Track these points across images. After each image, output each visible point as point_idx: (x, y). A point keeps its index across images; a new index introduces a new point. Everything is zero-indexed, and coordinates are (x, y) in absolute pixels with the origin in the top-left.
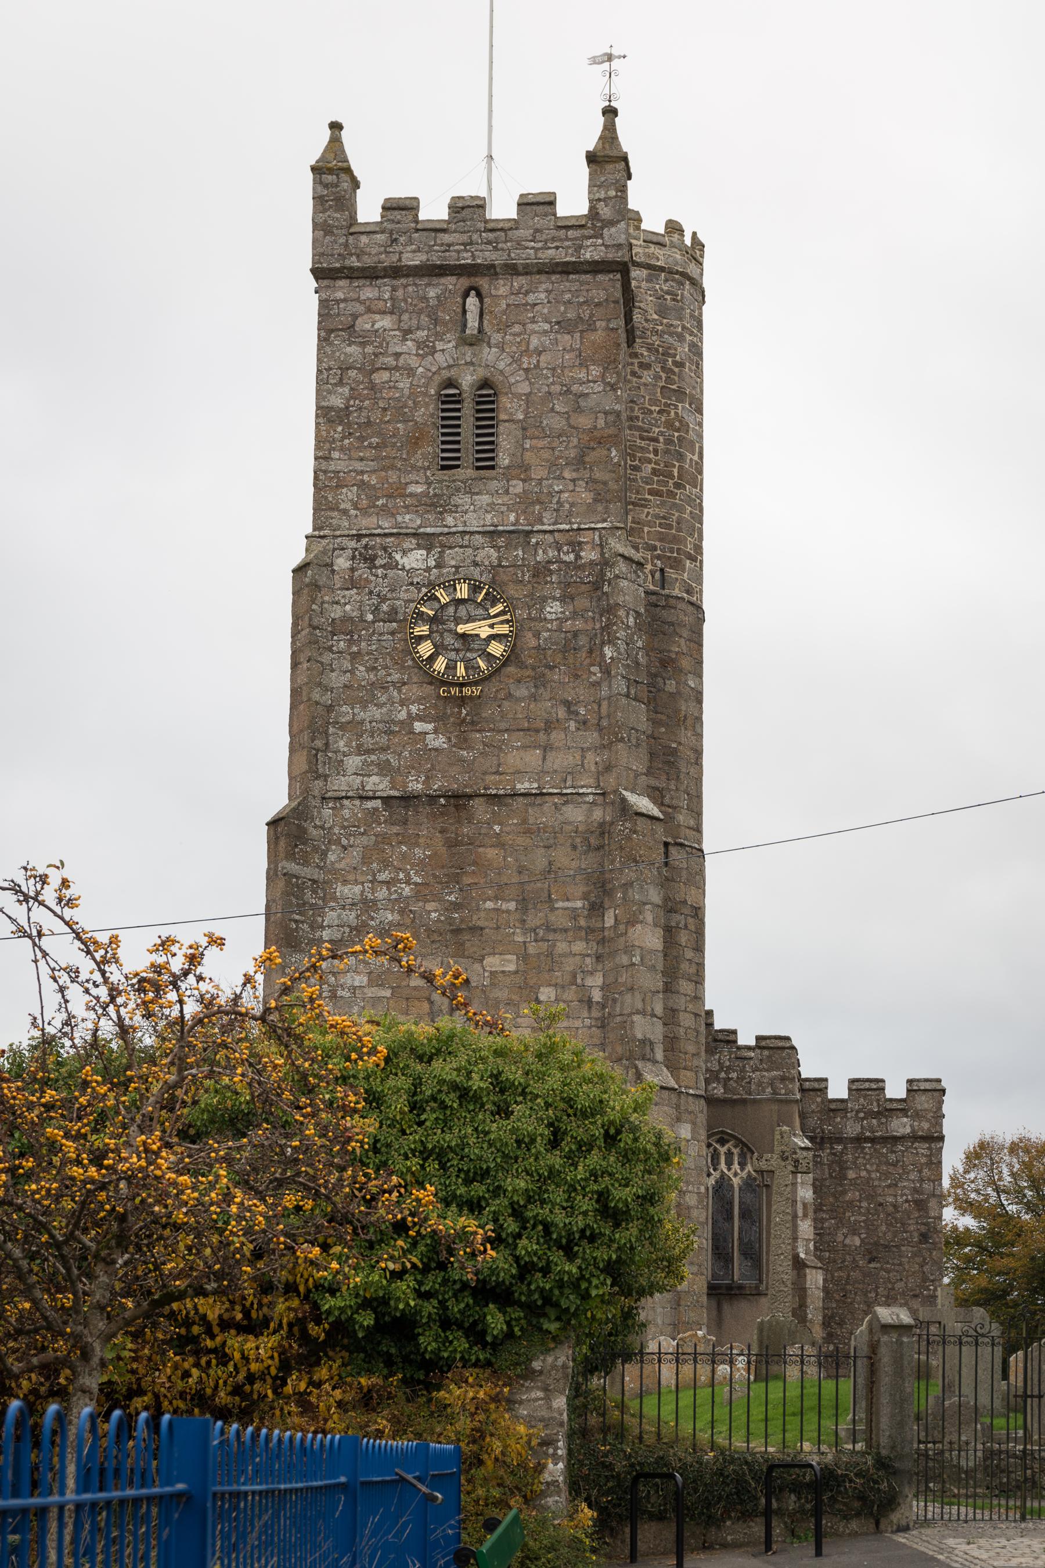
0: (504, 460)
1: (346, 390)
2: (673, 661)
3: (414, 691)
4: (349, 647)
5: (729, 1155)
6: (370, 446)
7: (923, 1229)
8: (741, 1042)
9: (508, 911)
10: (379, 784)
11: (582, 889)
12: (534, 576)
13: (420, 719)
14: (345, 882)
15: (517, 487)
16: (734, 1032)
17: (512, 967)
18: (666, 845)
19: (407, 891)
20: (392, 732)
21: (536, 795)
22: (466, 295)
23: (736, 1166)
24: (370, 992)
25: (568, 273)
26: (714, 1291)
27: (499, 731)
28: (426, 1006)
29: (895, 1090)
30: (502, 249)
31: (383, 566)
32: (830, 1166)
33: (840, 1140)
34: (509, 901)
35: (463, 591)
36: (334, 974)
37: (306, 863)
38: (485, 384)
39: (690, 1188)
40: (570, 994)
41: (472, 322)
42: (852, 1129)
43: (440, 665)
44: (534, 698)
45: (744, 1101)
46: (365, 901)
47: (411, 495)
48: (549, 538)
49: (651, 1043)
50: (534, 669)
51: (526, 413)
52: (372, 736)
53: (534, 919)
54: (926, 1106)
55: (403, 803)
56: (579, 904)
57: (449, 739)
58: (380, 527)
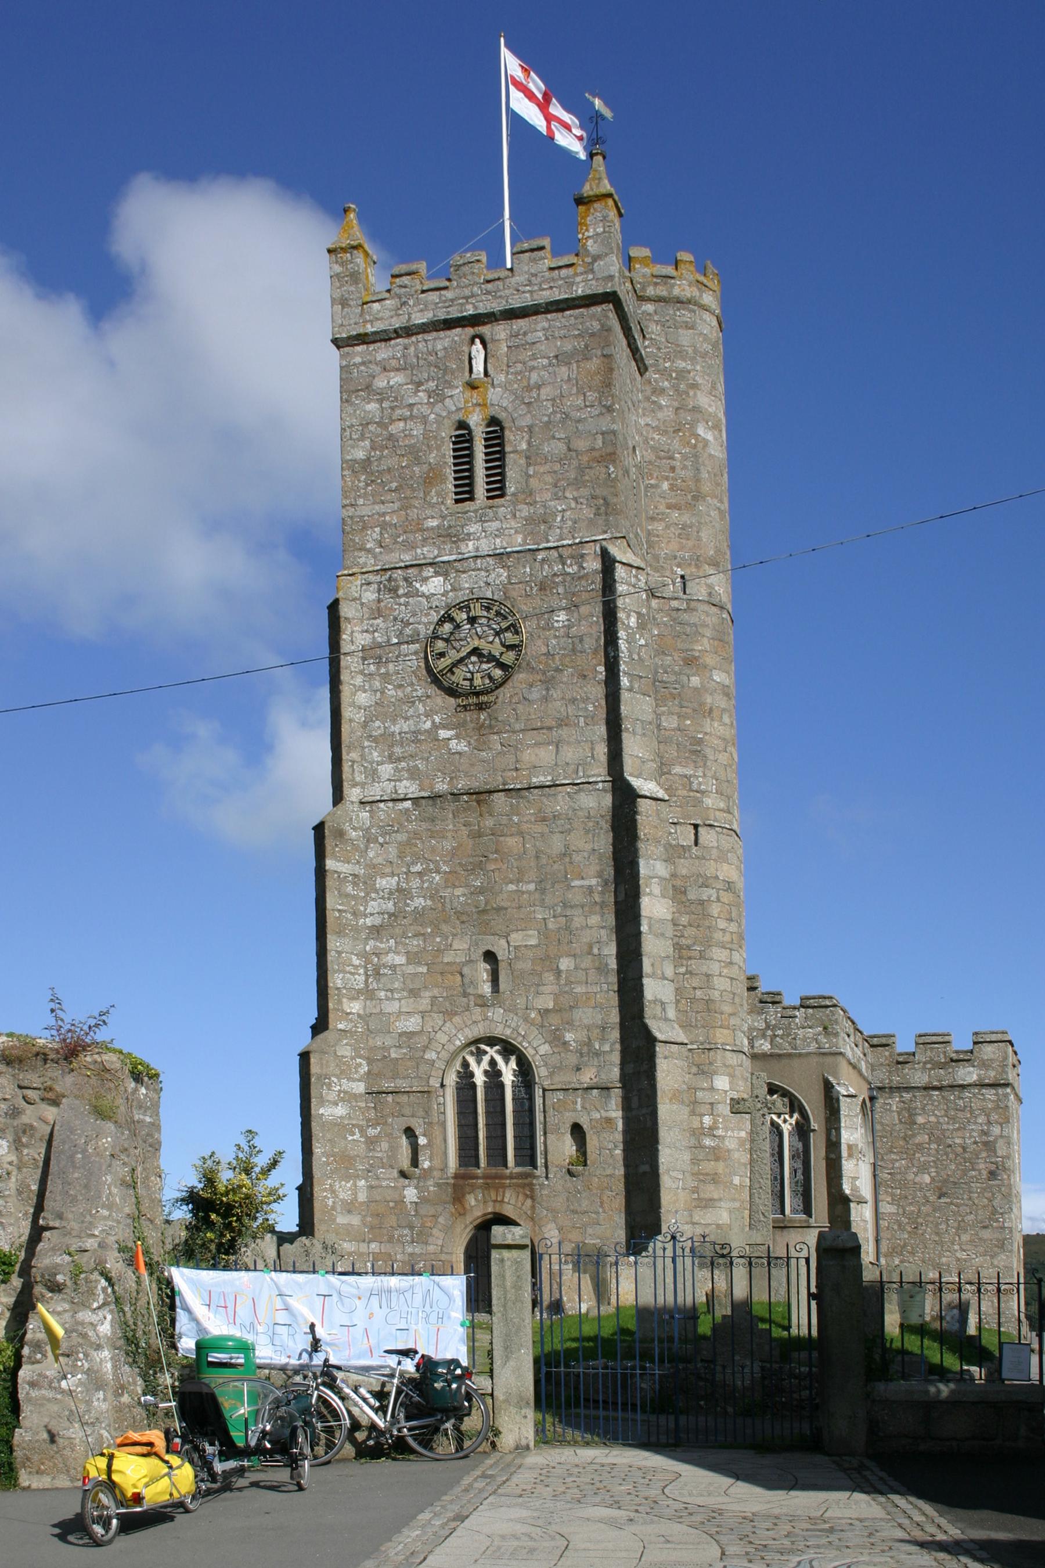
0: (511, 488)
1: (367, 443)
2: (696, 658)
4: (378, 669)
6: (391, 491)
7: (993, 1167)
8: (786, 1002)
9: (529, 892)
10: (409, 787)
12: (541, 590)
13: (445, 727)
14: (384, 875)
15: (524, 511)
18: (696, 826)
20: (419, 741)
21: (549, 787)
22: (472, 342)
24: (410, 969)
25: (563, 310)
27: (514, 732)
28: (459, 978)
30: (500, 297)
31: (406, 595)
32: (899, 1113)
33: (908, 1089)
34: (530, 882)
36: (377, 955)
39: (729, 1133)
40: (587, 962)
41: (479, 366)
44: (546, 699)
45: (790, 1055)
46: (399, 890)
47: (428, 529)
48: (554, 554)
49: (662, 1003)
50: (544, 673)
51: (529, 443)
52: (402, 746)
54: (992, 1056)
55: (430, 802)
56: (594, 882)
57: (469, 743)
58: (402, 561)
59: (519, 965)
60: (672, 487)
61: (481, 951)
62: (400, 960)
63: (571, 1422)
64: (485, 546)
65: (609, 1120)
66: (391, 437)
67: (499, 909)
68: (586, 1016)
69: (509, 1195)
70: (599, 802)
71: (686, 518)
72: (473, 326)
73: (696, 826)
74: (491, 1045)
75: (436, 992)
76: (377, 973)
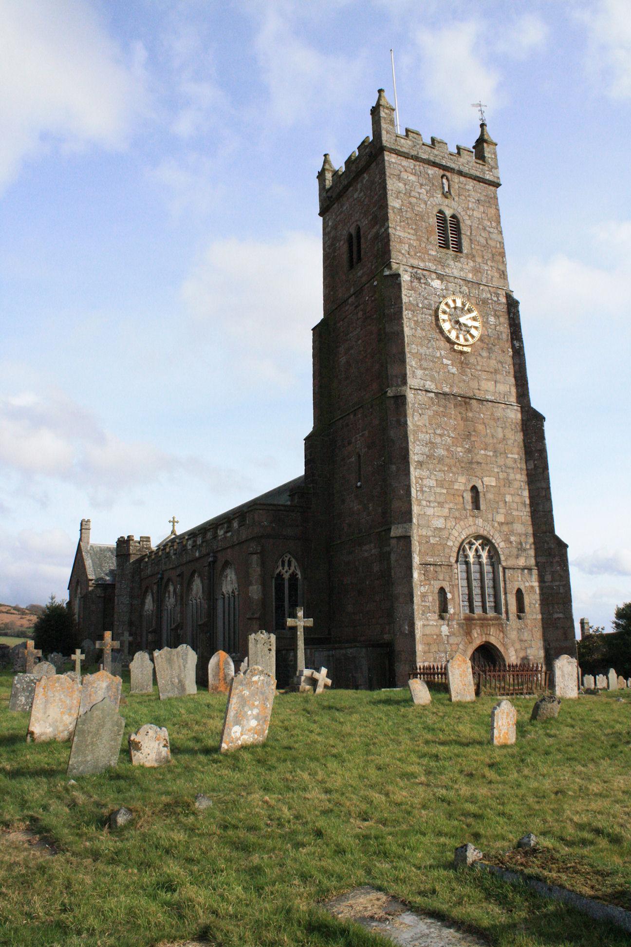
0: (465, 251)
23: (286, 568)
28: (461, 499)
41: (446, 189)
61: (471, 485)
63: (173, 541)
65: (532, 587)
67: (478, 463)
69: (492, 630)
70: (515, 415)
72: (444, 170)
75: (451, 505)
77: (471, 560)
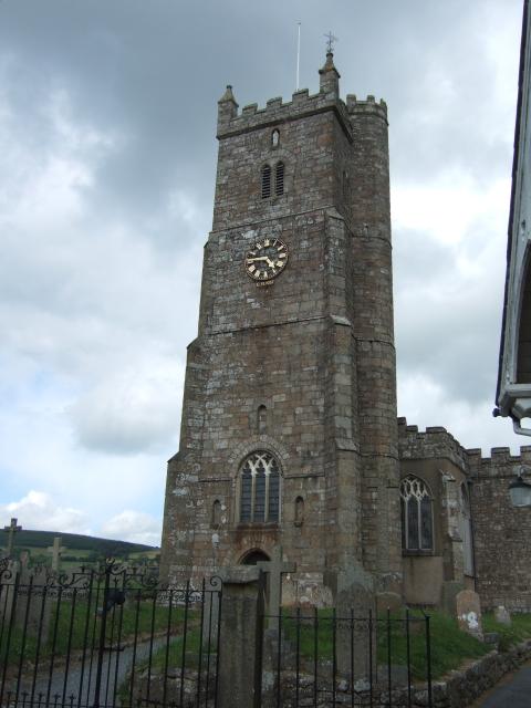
0: (286, 190)
3: (248, 286)
5: (415, 486)
10: (232, 326)
11: (315, 361)
13: (250, 297)
15: (291, 199)
16: (416, 427)
17: (283, 400)
19: (241, 370)
22: (273, 132)
26: (406, 554)
28: (247, 420)
29: (486, 454)
35: (267, 243)
37: (200, 362)
38: (280, 163)
41: (275, 142)
42: (494, 472)
43: (257, 274)
44: (296, 282)
53: (294, 377)
56: (314, 368)
59: (276, 412)
60: (363, 189)
62: (220, 411)
64: (273, 215)
66: (238, 174)
68: (307, 437)
71: (369, 202)
73: (371, 342)
74: (260, 454)
76: (209, 419)
77: (254, 472)
